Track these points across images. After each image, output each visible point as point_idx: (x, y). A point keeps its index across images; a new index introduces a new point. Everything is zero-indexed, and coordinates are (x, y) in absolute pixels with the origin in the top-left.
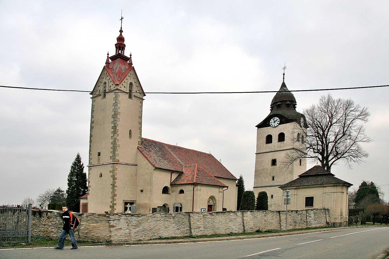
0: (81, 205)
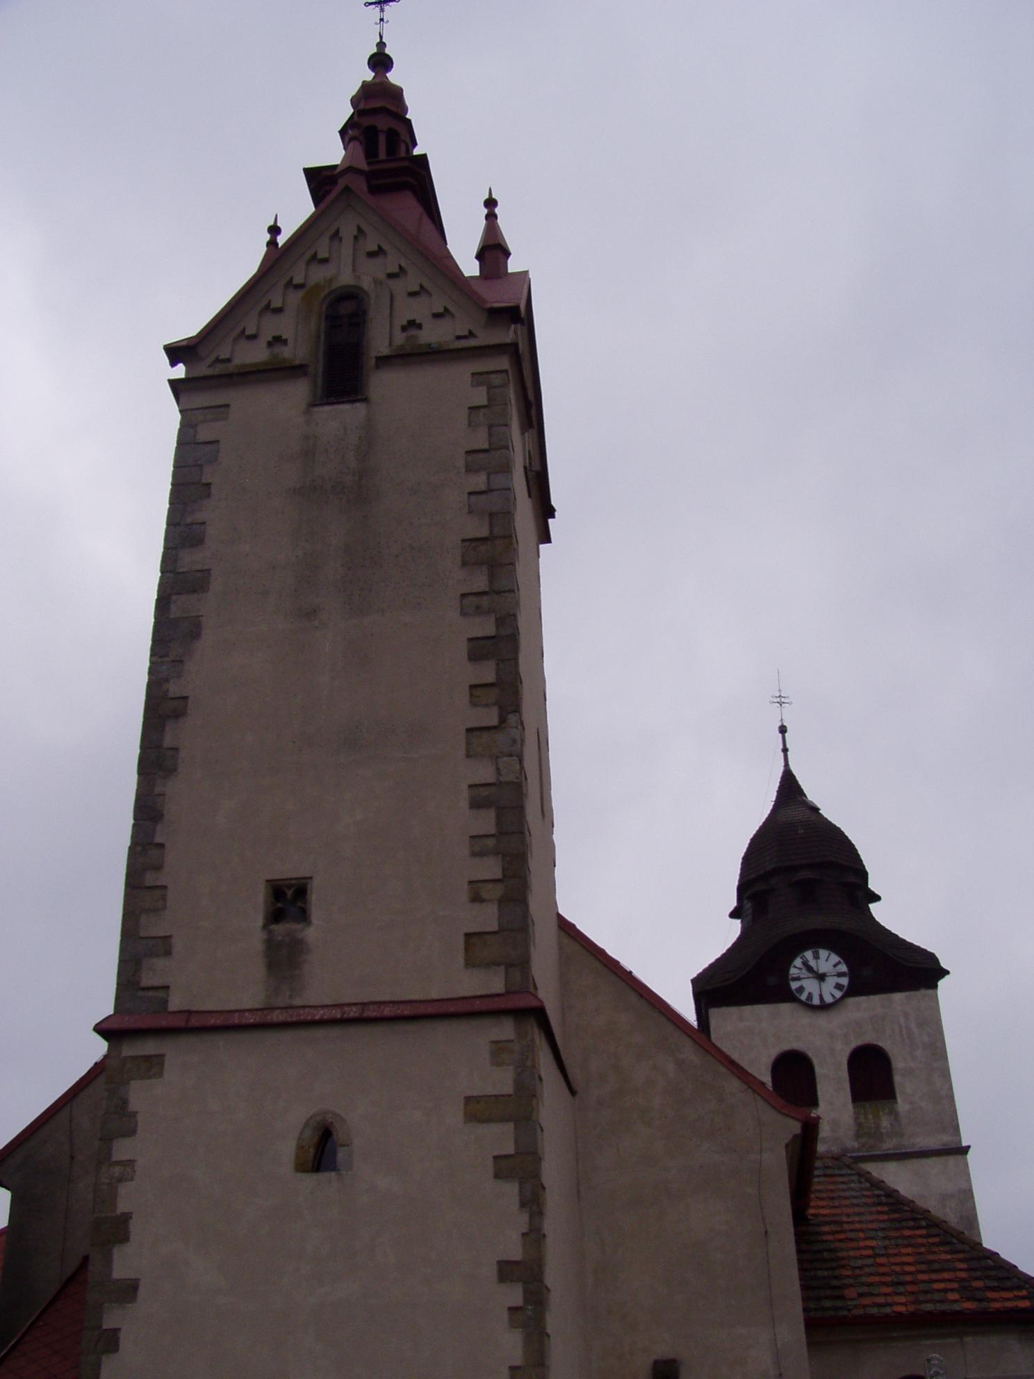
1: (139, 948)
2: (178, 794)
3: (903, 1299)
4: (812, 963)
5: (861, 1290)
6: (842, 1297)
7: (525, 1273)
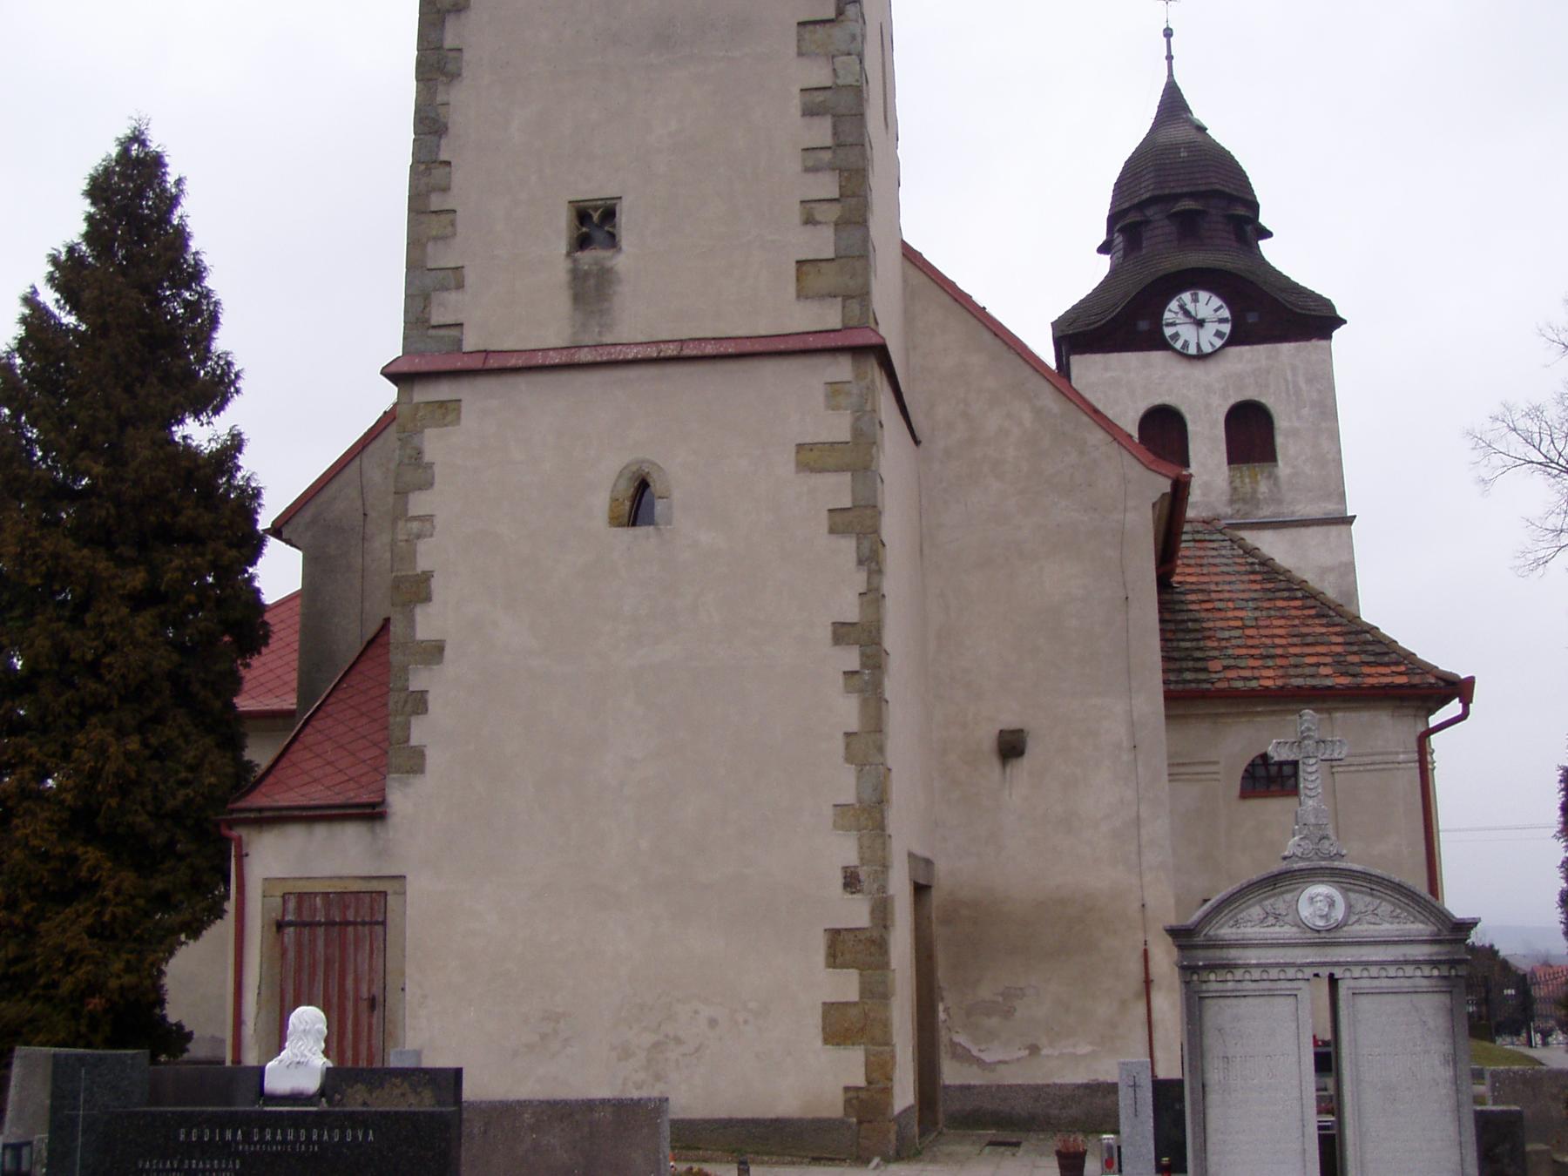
0: (437, 1109)
1: (427, 281)
2: (465, 103)
3: (1270, 673)
4: (1190, 307)
5: (1225, 662)
6: (1205, 670)
7: (862, 635)
